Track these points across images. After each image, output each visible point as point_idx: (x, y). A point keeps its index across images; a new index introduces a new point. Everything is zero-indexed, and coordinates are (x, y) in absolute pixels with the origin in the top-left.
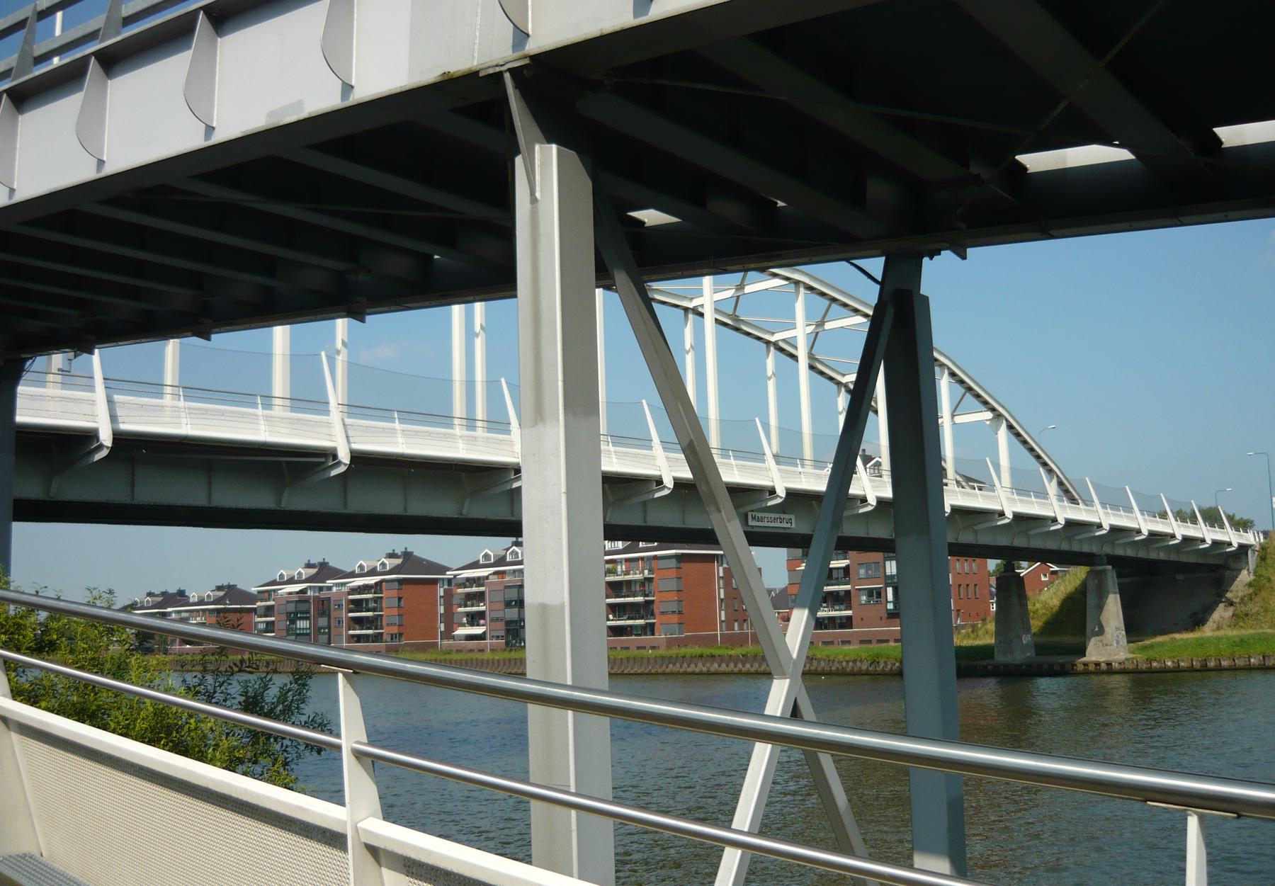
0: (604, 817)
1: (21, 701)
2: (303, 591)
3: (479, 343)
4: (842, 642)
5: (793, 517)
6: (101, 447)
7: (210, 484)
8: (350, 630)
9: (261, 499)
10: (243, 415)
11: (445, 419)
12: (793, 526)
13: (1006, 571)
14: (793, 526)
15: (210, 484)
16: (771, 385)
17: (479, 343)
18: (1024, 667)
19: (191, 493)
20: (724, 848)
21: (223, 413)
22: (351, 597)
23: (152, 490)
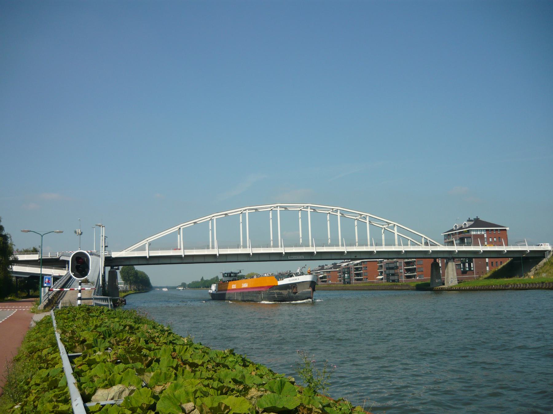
0: (26, 302)
1: (214, 278)
2: (348, 265)
3: (210, 228)
4: (253, 277)
5: (303, 256)
6: (375, 253)
7: (259, 257)
8: (404, 267)
9: (268, 259)
10: (381, 247)
11: (308, 246)
12: (303, 258)
13: (434, 262)
14: (303, 258)
15: (259, 257)
16: (328, 222)
17: (210, 228)
18: (165, 290)
19: (169, 261)
20: (460, 281)
21: (301, 248)
22: (354, 267)
23: (324, 257)
